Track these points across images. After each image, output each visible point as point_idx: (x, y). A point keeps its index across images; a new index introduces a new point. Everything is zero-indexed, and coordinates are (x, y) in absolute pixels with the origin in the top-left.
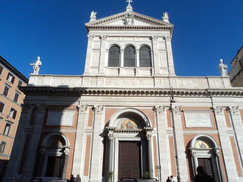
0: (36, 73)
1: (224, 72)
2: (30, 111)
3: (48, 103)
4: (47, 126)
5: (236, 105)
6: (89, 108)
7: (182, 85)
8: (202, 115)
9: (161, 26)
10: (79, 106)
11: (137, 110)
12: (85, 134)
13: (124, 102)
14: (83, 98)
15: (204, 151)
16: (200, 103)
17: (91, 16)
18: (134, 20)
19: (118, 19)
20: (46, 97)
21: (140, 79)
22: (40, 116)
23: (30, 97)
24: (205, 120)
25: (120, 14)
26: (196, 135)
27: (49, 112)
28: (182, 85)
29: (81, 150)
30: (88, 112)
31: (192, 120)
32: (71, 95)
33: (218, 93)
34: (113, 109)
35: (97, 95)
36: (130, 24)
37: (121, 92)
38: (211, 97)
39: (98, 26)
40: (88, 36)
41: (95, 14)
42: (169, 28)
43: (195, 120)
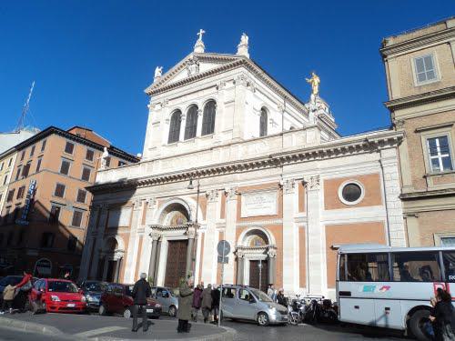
0: (103, 167)
2: (96, 213)
3: (110, 202)
5: (313, 174)
7: (246, 153)
8: (265, 196)
12: (137, 234)
15: (258, 251)
17: (156, 75)
20: (108, 196)
22: (103, 217)
23: (101, 197)
24: (268, 204)
26: (245, 227)
28: (246, 153)
30: (296, 190)
32: (124, 190)
37: (171, 178)
38: (379, 151)
40: (149, 106)
43: (253, 206)
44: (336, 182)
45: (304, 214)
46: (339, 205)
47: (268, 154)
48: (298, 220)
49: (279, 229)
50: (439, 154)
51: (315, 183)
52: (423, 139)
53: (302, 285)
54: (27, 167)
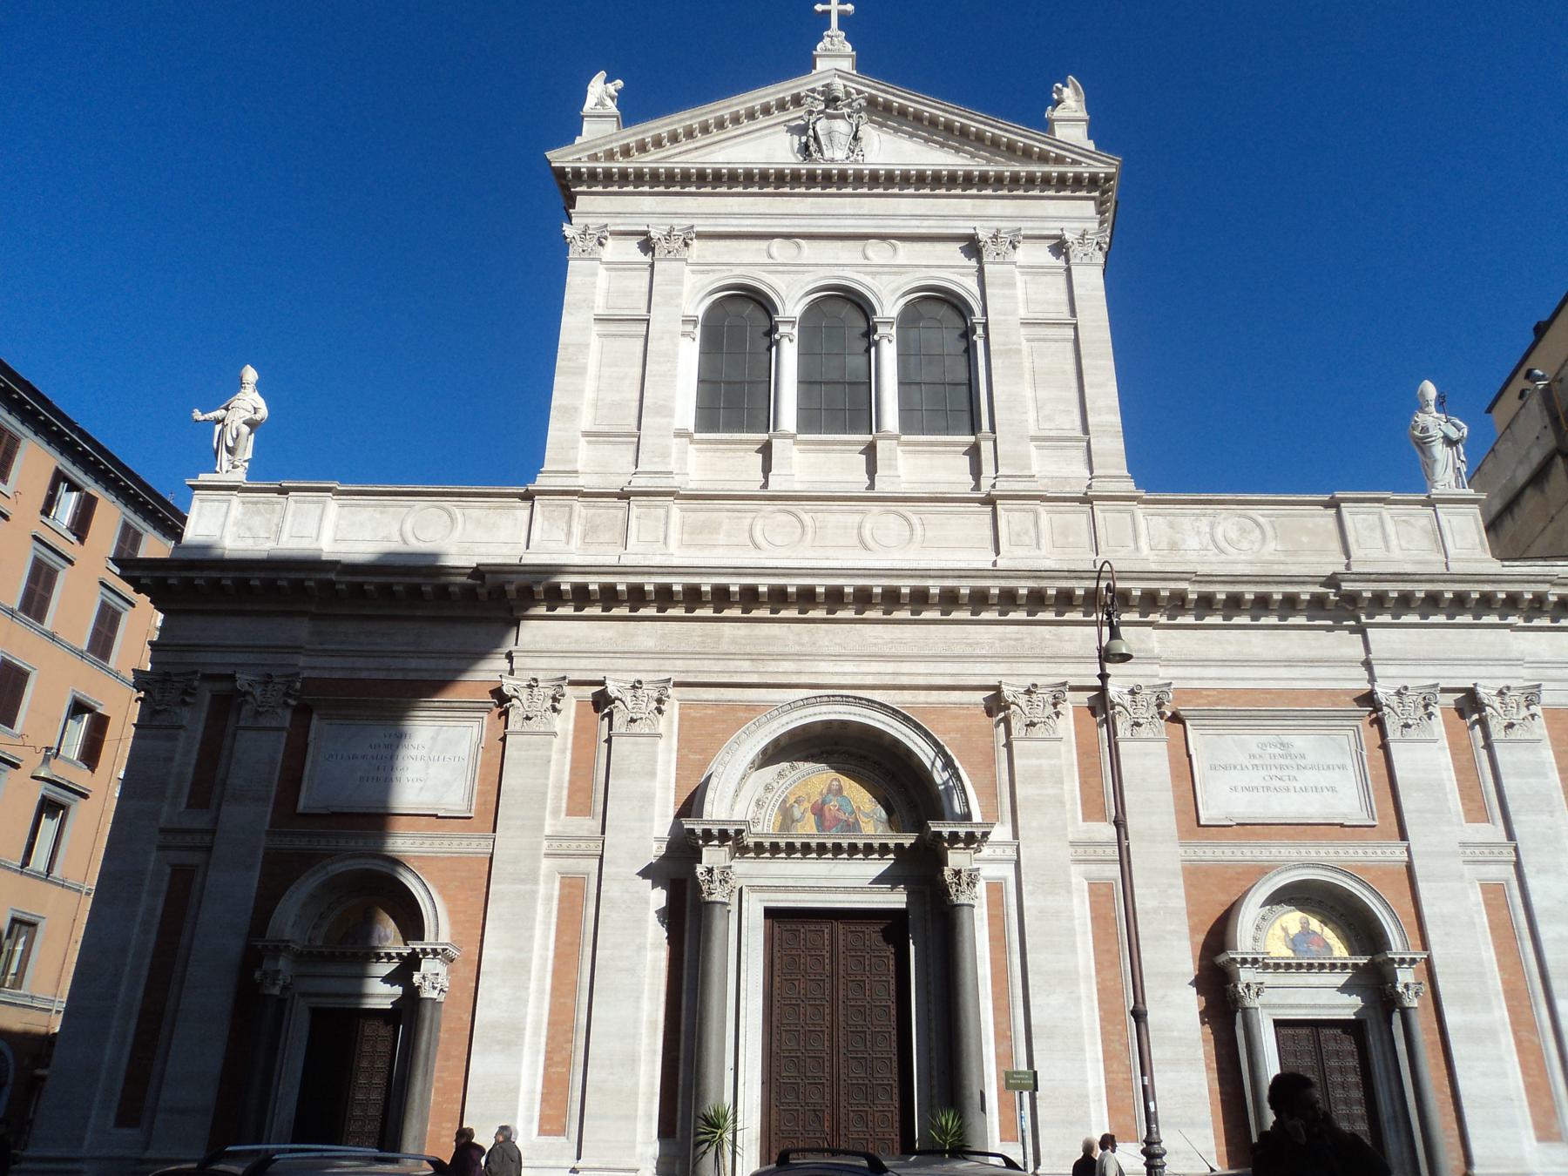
1: (1446, 468)
2: (194, 720)
5: (1521, 677)
7: (1173, 546)
8: (1302, 741)
9: (1038, 169)
10: (507, 690)
11: (871, 703)
12: (546, 864)
13: (798, 657)
15: (1314, 979)
16: (1290, 663)
17: (590, 104)
18: (869, 132)
19: (762, 121)
20: (301, 630)
23: (196, 629)
26: (1263, 871)
28: (1173, 546)
29: (522, 967)
30: (564, 723)
33: (1405, 602)
34: (732, 706)
36: (836, 156)
38: (1361, 630)
39: (630, 165)
40: (568, 230)
41: (611, 88)
42: (1094, 181)
43: (1256, 778)
45: (201, 820)
48: (1474, 853)
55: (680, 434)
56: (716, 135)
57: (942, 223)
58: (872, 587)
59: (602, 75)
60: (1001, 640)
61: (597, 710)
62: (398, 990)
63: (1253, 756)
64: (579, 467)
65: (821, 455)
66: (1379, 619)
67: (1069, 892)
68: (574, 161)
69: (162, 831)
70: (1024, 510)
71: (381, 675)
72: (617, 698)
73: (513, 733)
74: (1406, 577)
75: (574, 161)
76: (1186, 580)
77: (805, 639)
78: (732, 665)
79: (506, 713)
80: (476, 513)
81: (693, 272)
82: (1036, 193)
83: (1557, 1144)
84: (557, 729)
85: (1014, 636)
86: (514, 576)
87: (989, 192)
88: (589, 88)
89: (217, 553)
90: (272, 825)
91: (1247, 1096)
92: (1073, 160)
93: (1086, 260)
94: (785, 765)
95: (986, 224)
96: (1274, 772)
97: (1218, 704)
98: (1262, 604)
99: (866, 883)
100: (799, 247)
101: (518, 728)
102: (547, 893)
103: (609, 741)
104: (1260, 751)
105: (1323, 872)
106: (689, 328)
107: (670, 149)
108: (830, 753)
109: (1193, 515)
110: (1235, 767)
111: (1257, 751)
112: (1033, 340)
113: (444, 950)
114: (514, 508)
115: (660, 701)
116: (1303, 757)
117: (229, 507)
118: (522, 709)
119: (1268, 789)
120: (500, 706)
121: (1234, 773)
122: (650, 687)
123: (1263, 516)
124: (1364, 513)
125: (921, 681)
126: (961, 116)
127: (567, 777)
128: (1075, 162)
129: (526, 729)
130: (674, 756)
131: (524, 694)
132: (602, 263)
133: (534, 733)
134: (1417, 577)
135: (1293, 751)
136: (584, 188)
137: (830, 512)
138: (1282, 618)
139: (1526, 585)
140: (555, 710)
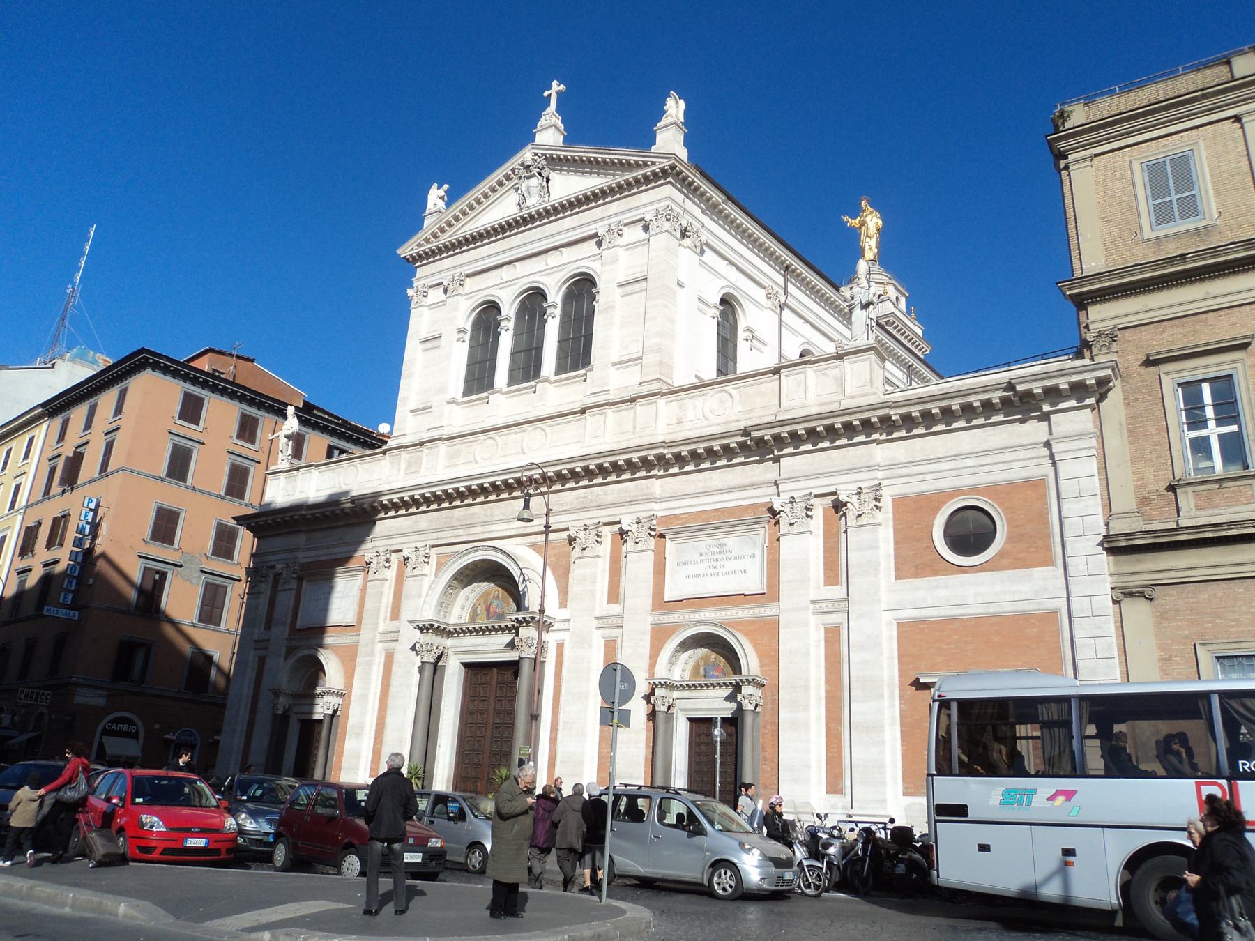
2: (266, 588)
3: (302, 557)
4: (299, 630)
5: (866, 480)
6: (820, 508)
8: (732, 542)
9: (638, 174)
10: (777, 507)
13: (483, 524)
14: (383, 527)
15: (711, 693)
16: (730, 490)
17: (430, 206)
18: (554, 176)
19: (501, 191)
20: (301, 539)
21: (542, 425)
23: (278, 543)
25: (499, 174)
27: (305, 585)
29: (364, 697)
31: (693, 570)
33: (795, 438)
35: (942, 427)
38: (1045, 417)
40: (410, 292)
41: (441, 192)
43: (700, 568)
44: (929, 502)
45: (837, 591)
46: (937, 567)
47: (741, 426)
49: (768, 633)
50: (1212, 424)
51: (383, 563)
52: (1168, 384)
53: (834, 786)
54: (75, 462)
55: (452, 402)
56: (479, 208)
57: (473, 265)
58: (931, 409)
59: (436, 185)
60: (577, 499)
61: (837, 512)
62: (734, 705)
63: (701, 555)
64: (407, 432)
65: (516, 398)
66: (786, 451)
67: (590, 646)
68: (410, 251)
69: (255, 641)
70: (599, 414)
71: (328, 557)
72: (780, 511)
73: (852, 527)
74: (789, 422)
75: (410, 251)
76: (660, 447)
77: (488, 513)
78: (456, 532)
79: (778, 522)
80: (366, 466)
81: (466, 299)
82: (635, 190)
83: (838, 795)
84: (388, 578)
85: (583, 495)
86: (365, 500)
87: (609, 199)
88: (429, 197)
89: (273, 506)
90: (290, 635)
91: (286, 756)
92: (651, 162)
93: (658, 230)
94: (475, 585)
95: (601, 224)
96: (713, 563)
97: (686, 523)
98: (646, 464)
99: (502, 647)
100: (561, 251)
101: (786, 531)
102: (379, 659)
103: (846, 532)
104: (706, 551)
105: (711, 627)
106: (462, 335)
107: (450, 231)
108: (493, 576)
109: (694, 396)
110: (691, 563)
111: (704, 550)
112: (625, 295)
113: (753, 680)
114: (379, 460)
115: (877, 499)
116: (731, 552)
117: (805, 376)
118: (855, 510)
119: (707, 575)
120: (774, 518)
121: (689, 566)
122: (646, 520)
123: (735, 389)
124: (794, 374)
125: (513, 533)
126: (593, 153)
127: (391, 601)
128: (653, 163)
129: (859, 523)
130: (392, 590)
131: (413, 556)
132: (621, 247)
133: (417, 576)
134: (797, 420)
135: (726, 548)
136: (419, 264)
137: (509, 434)
138: (948, 424)
139: (872, 412)
140: (808, 516)
